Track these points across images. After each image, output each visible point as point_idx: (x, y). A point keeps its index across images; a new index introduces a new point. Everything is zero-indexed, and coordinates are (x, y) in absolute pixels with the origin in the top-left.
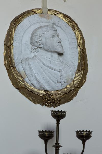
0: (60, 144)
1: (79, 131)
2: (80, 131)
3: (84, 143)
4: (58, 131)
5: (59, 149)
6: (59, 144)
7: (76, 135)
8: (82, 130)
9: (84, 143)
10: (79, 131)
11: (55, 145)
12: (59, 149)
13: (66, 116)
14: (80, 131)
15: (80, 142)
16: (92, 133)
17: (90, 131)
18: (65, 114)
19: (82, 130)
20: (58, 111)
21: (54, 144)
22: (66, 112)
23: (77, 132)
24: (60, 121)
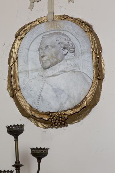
0: (21, 163)
1: (9, 126)
2: (11, 125)
3: (39, 161)
4: (17, 150)
5: (20, 169)
6: (20, 163)
7: (7, 131)
8: (12, 125)
9: (39, 161)
10: (9, 126)
11: (16, 164)
12: (20, 168)
13: (24, 130)
14: (11, 125)
15: (12, 138)
16: (49, 150)
17: (22, 125)
18: (47, 152)
19: (12, 125)
20: (41, 148)
21: (14, 163)
22: (23, 126)
23: (8, 127)
24: (41, 159)
